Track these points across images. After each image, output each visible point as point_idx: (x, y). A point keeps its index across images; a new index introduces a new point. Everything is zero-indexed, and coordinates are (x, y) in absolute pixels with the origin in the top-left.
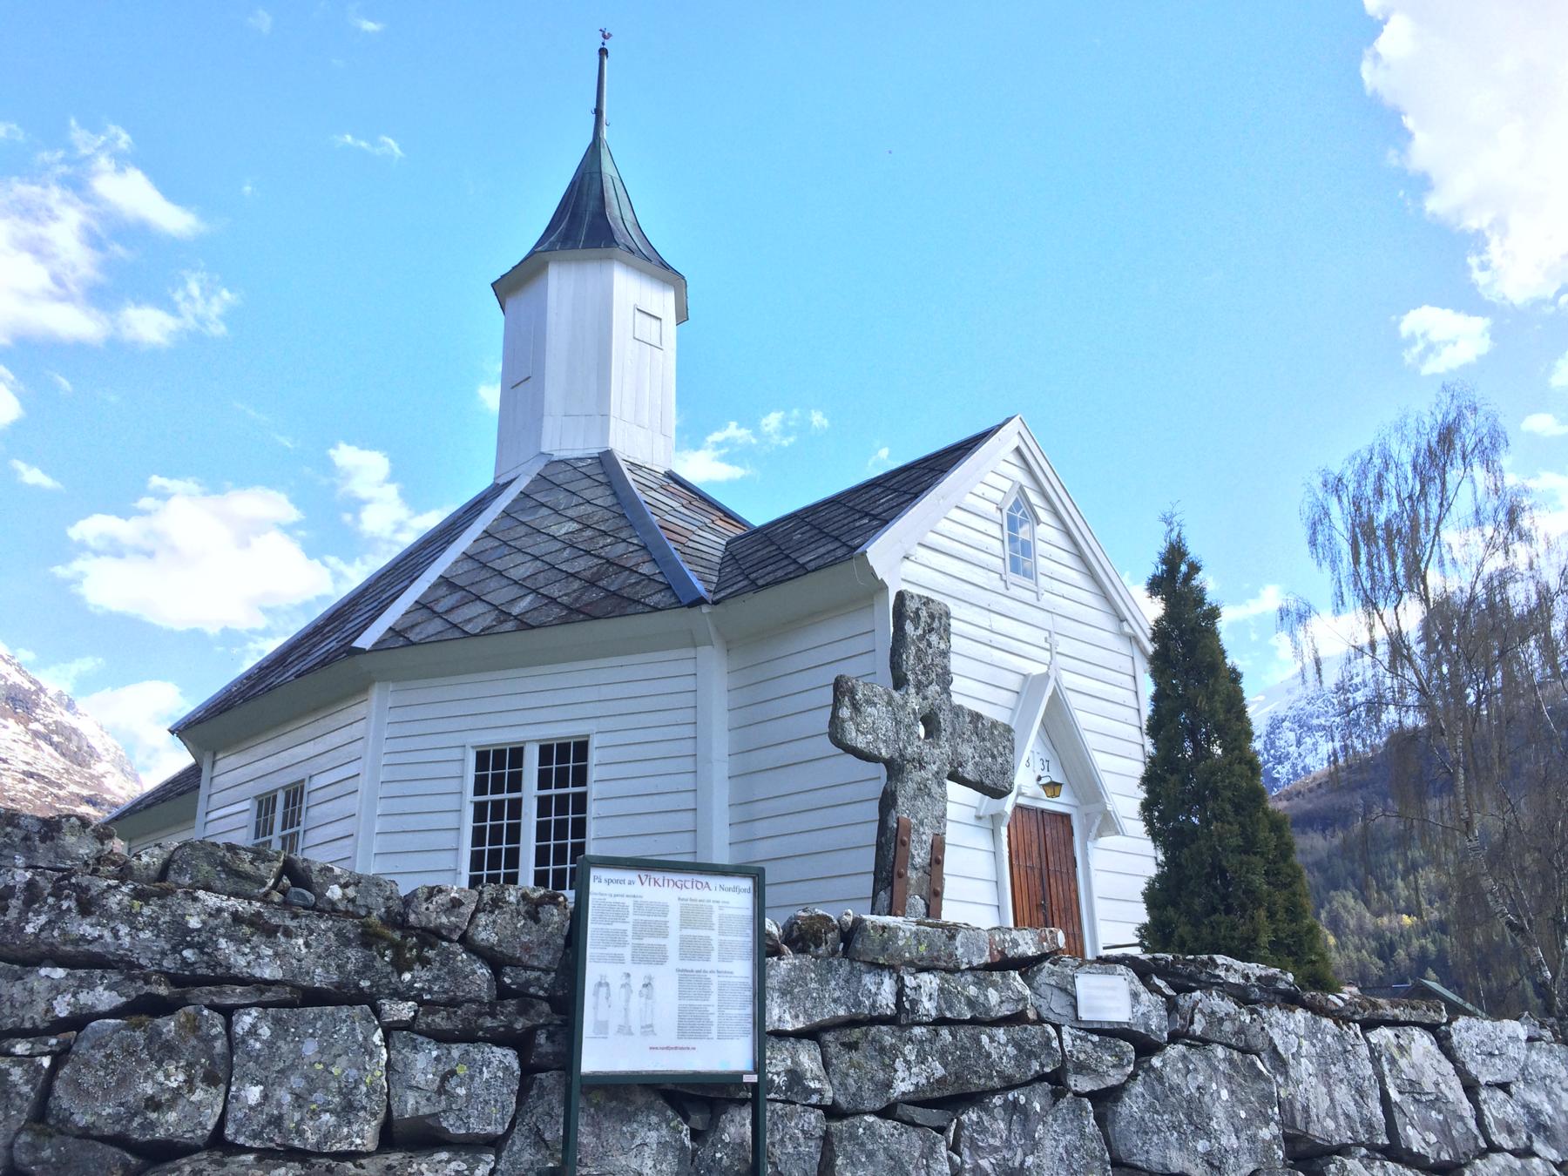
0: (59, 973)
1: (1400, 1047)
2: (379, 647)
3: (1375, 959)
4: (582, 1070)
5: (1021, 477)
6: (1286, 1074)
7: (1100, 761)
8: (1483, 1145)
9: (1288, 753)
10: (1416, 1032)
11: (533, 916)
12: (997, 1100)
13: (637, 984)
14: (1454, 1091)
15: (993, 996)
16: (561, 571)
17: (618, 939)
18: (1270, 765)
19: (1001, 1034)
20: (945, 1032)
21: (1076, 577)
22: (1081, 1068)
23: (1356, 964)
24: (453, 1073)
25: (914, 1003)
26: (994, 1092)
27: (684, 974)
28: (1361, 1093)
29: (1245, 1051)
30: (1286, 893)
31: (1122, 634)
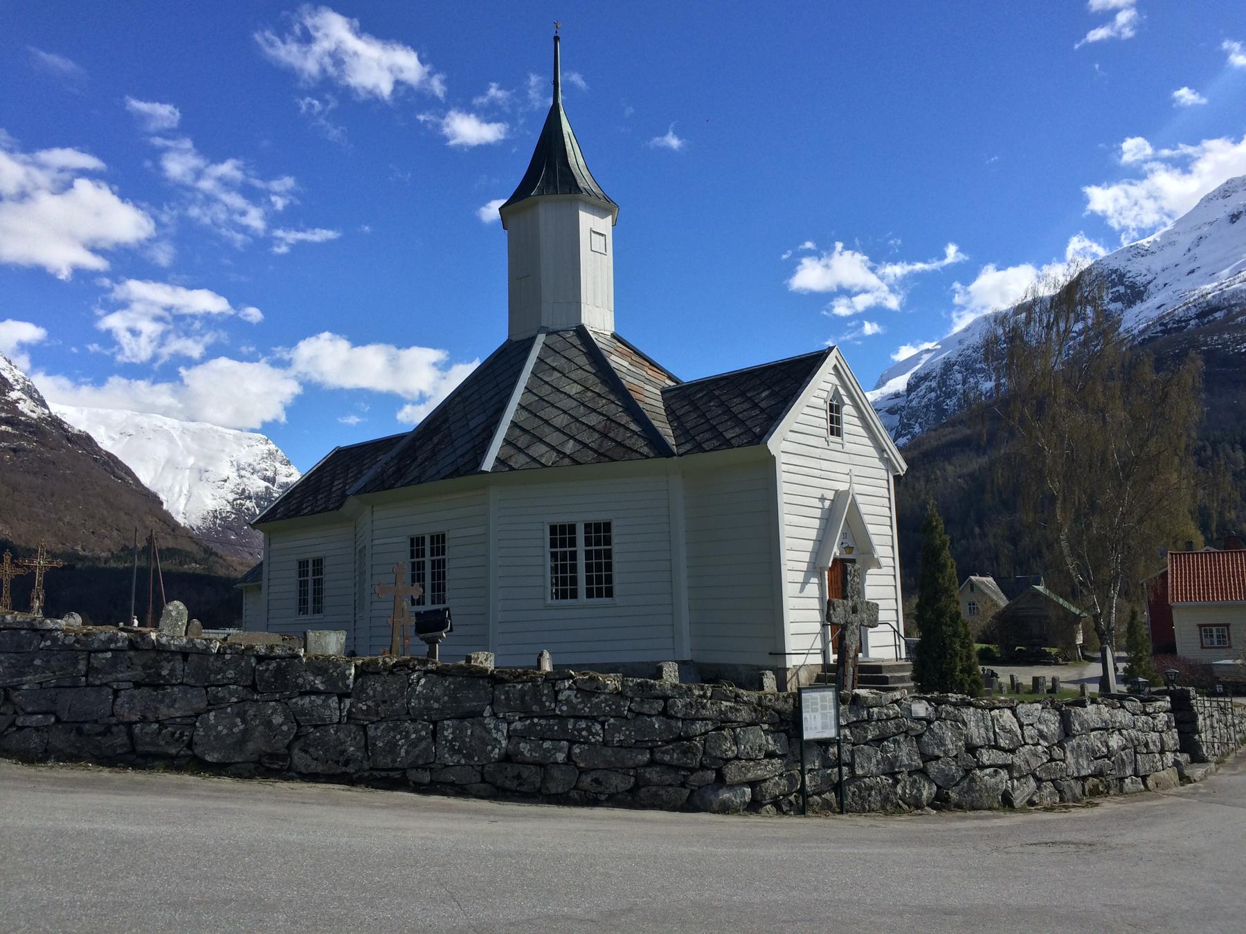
1: (1000, 716)
3: (1008, 544)
4: (805, 738)
5: (836, 381)
7: (871, 529)
8: (1023, 743)
9: (956, 390)
10: (1006, 710)
11: (786, 702)
14: (1016, 727)
15: (891, 712)
16: (583, 424)
18: (941, 399)
21: (861, 431)
23: (993, 547)
28: (987, 730)
30: (966, 650)
31: (882, 459)
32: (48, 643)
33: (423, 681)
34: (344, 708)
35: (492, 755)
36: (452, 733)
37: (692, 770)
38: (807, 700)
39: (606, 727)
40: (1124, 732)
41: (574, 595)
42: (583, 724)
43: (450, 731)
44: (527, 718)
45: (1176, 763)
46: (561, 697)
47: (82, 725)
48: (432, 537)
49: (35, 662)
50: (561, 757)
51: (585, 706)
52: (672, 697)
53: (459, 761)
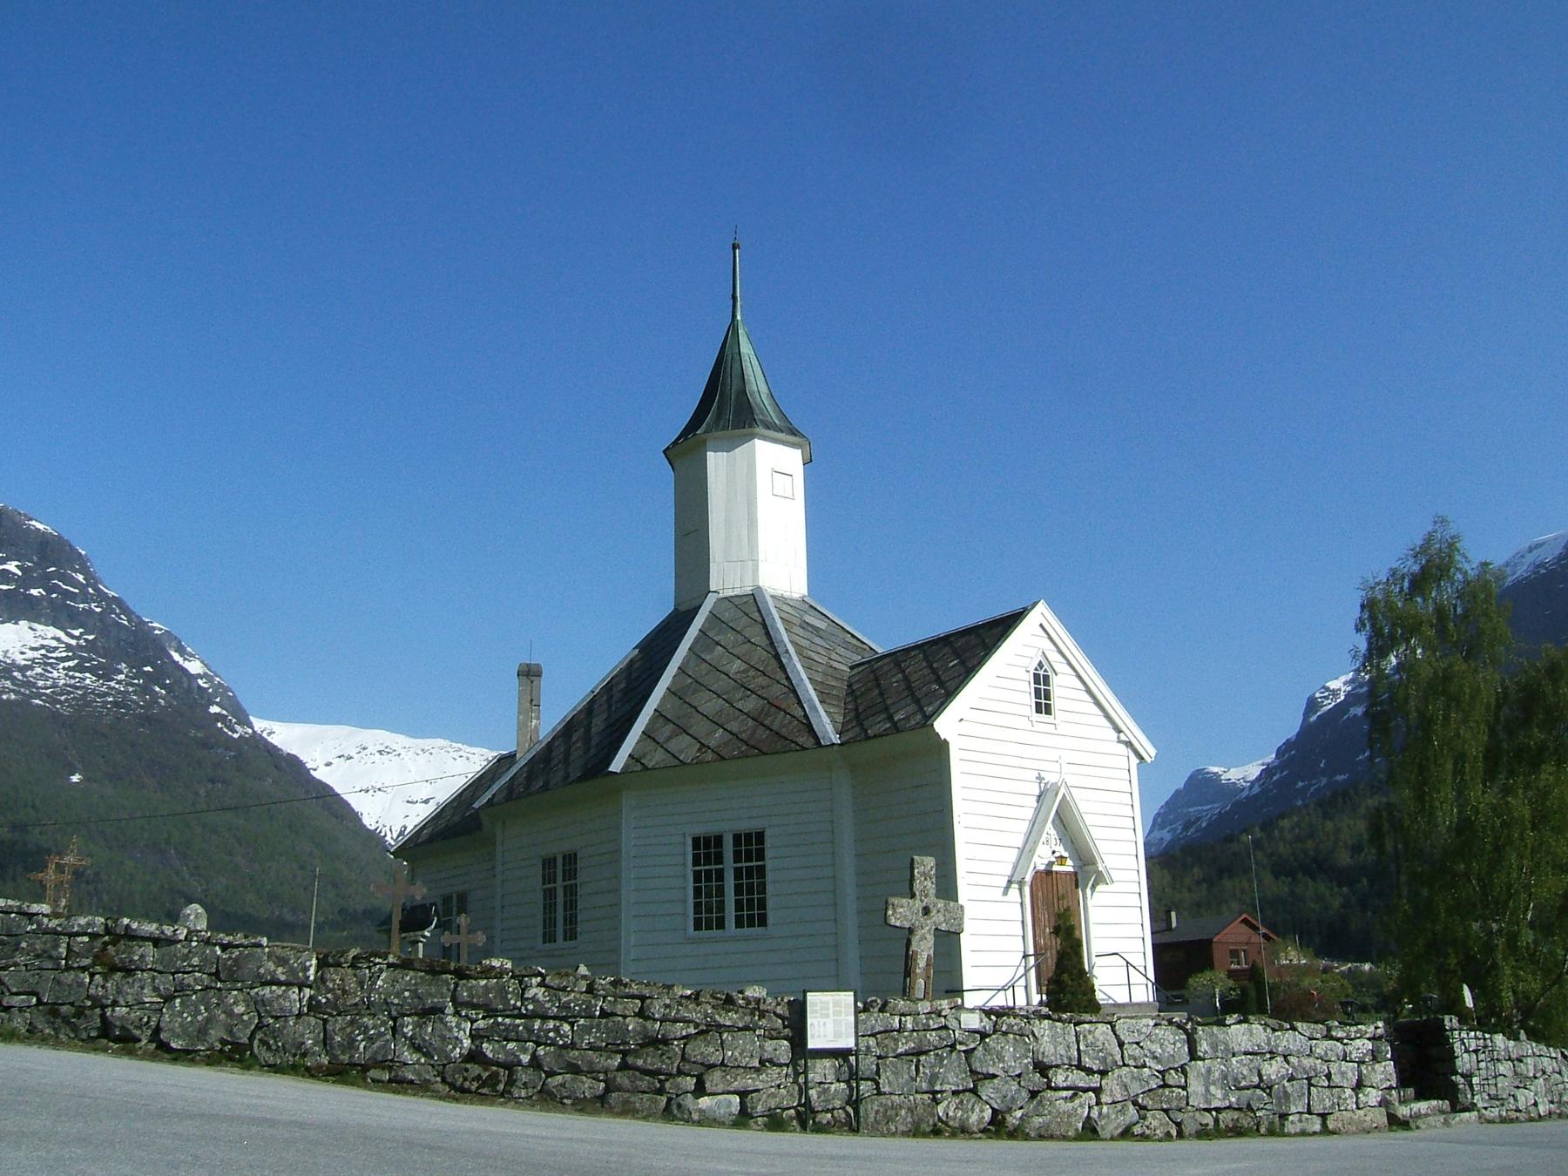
0: (681, 1024)
2: (626, 770)
6: (1037, 1042)
12: (932, 1053)
13: (821, 1024)
17: (816, 1012)
19: (934, 1033)
20: (915, 1034)
22: (960, 1043)
24: (1098, 1103)
25: (905, 1025)
26: (931, 1051)
27: (835, 1021)
29: (1021, 1035)
32: (34, 927)
33: (383, 975)
34: (304, 998)
35: (452, 1055)
36: (412, 1030)
37: (670, 1075)
38: (815, 1004)
39: (575, 1028)
40: (1291, 1059)
41: (721, 924)
42: (551, 1024)
43: (410, 1027)
44: (491, 1017)
45: (1384, 1103)
46: (530, 994)
47: (60, 1007)
48: (564, 858)
49: (22, 945)
50: (525, 1058)
51: (553, 1005)
52: (649, 998)
53: (419, 1059)
